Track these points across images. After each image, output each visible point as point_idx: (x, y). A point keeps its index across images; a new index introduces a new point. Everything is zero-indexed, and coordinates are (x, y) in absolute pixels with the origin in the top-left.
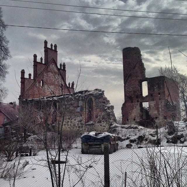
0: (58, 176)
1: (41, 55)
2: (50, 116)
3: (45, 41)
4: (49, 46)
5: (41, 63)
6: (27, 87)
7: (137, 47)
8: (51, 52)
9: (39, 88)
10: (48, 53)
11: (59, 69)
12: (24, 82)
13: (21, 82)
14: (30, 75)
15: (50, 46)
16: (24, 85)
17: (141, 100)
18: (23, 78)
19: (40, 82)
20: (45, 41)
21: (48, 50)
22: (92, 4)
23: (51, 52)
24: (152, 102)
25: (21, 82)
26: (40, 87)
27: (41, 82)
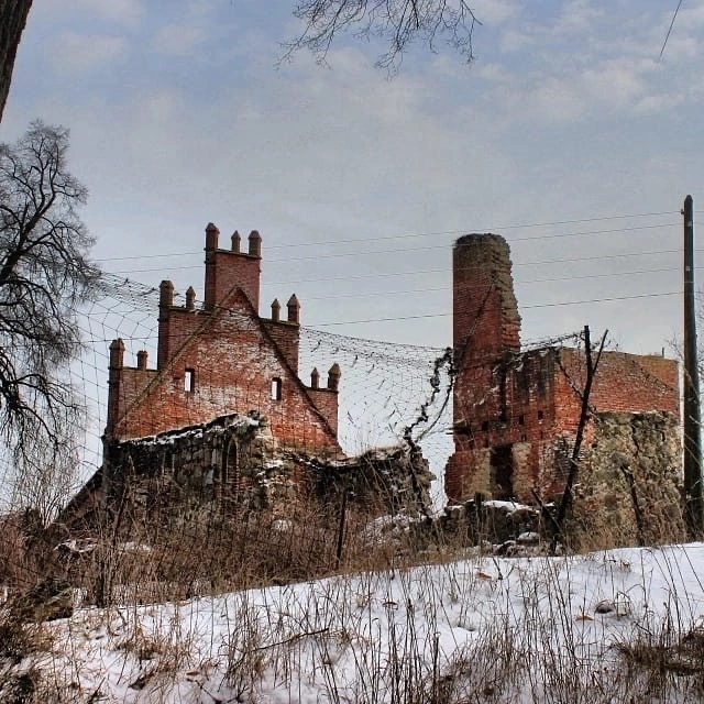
0: (391, 352)
1: (190, 278)
2: (211, 485)
3: (211, 225)
4: (224, 244)
5: (186, 311)
6: (129, 395)
7: (503, 236)
8: (232, 265)
9: (176, 398)
10: (218, 270)
11: (262, 323)
12: (118, 383)
13: (108, 382)
14: (142, 356)
15: (231, 242)
16: (118, 392)
17: (494, 438)
18: (116, 369)
19: (178, 378)
20: (211, 225)
21: (218, 261)
22: (475, 635)
23: (232, 265)
24: (532, 439)
25: (108, 382)
26: (182, 396)
27: (184, 376)
